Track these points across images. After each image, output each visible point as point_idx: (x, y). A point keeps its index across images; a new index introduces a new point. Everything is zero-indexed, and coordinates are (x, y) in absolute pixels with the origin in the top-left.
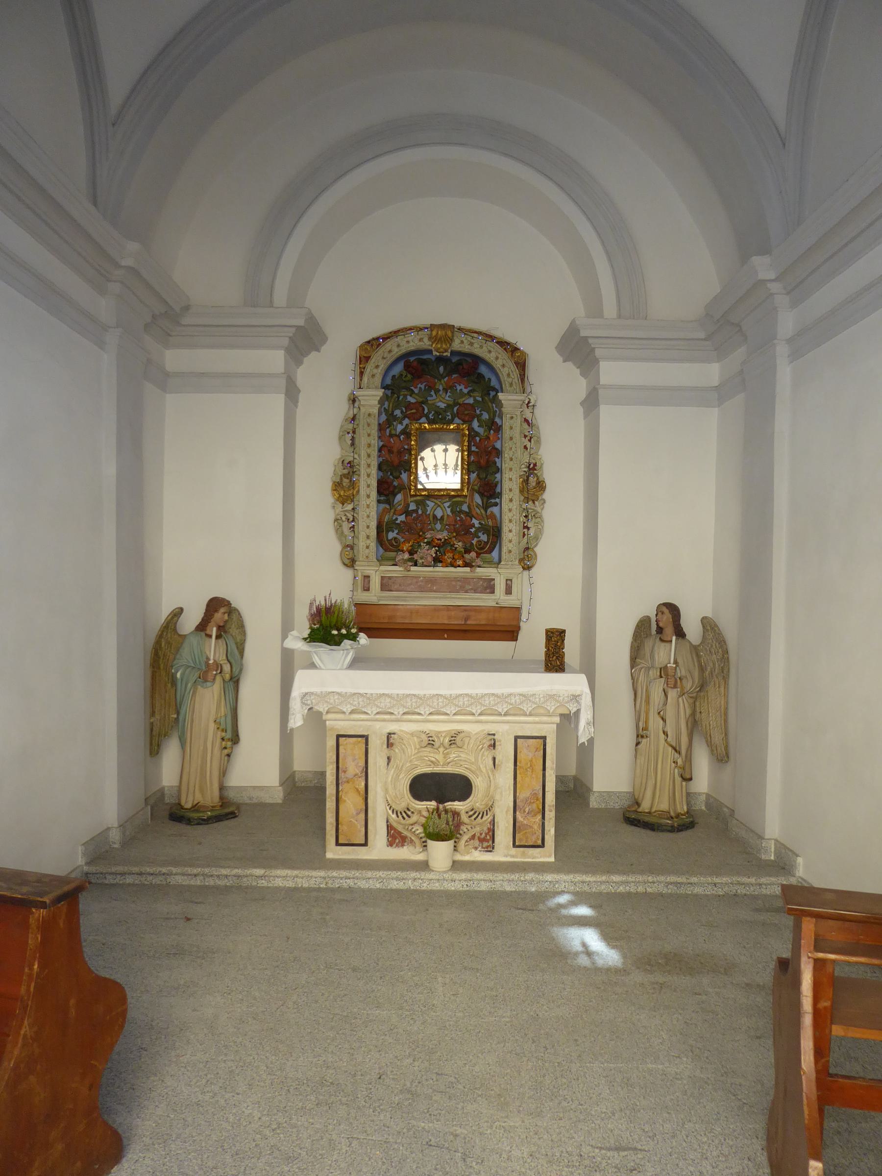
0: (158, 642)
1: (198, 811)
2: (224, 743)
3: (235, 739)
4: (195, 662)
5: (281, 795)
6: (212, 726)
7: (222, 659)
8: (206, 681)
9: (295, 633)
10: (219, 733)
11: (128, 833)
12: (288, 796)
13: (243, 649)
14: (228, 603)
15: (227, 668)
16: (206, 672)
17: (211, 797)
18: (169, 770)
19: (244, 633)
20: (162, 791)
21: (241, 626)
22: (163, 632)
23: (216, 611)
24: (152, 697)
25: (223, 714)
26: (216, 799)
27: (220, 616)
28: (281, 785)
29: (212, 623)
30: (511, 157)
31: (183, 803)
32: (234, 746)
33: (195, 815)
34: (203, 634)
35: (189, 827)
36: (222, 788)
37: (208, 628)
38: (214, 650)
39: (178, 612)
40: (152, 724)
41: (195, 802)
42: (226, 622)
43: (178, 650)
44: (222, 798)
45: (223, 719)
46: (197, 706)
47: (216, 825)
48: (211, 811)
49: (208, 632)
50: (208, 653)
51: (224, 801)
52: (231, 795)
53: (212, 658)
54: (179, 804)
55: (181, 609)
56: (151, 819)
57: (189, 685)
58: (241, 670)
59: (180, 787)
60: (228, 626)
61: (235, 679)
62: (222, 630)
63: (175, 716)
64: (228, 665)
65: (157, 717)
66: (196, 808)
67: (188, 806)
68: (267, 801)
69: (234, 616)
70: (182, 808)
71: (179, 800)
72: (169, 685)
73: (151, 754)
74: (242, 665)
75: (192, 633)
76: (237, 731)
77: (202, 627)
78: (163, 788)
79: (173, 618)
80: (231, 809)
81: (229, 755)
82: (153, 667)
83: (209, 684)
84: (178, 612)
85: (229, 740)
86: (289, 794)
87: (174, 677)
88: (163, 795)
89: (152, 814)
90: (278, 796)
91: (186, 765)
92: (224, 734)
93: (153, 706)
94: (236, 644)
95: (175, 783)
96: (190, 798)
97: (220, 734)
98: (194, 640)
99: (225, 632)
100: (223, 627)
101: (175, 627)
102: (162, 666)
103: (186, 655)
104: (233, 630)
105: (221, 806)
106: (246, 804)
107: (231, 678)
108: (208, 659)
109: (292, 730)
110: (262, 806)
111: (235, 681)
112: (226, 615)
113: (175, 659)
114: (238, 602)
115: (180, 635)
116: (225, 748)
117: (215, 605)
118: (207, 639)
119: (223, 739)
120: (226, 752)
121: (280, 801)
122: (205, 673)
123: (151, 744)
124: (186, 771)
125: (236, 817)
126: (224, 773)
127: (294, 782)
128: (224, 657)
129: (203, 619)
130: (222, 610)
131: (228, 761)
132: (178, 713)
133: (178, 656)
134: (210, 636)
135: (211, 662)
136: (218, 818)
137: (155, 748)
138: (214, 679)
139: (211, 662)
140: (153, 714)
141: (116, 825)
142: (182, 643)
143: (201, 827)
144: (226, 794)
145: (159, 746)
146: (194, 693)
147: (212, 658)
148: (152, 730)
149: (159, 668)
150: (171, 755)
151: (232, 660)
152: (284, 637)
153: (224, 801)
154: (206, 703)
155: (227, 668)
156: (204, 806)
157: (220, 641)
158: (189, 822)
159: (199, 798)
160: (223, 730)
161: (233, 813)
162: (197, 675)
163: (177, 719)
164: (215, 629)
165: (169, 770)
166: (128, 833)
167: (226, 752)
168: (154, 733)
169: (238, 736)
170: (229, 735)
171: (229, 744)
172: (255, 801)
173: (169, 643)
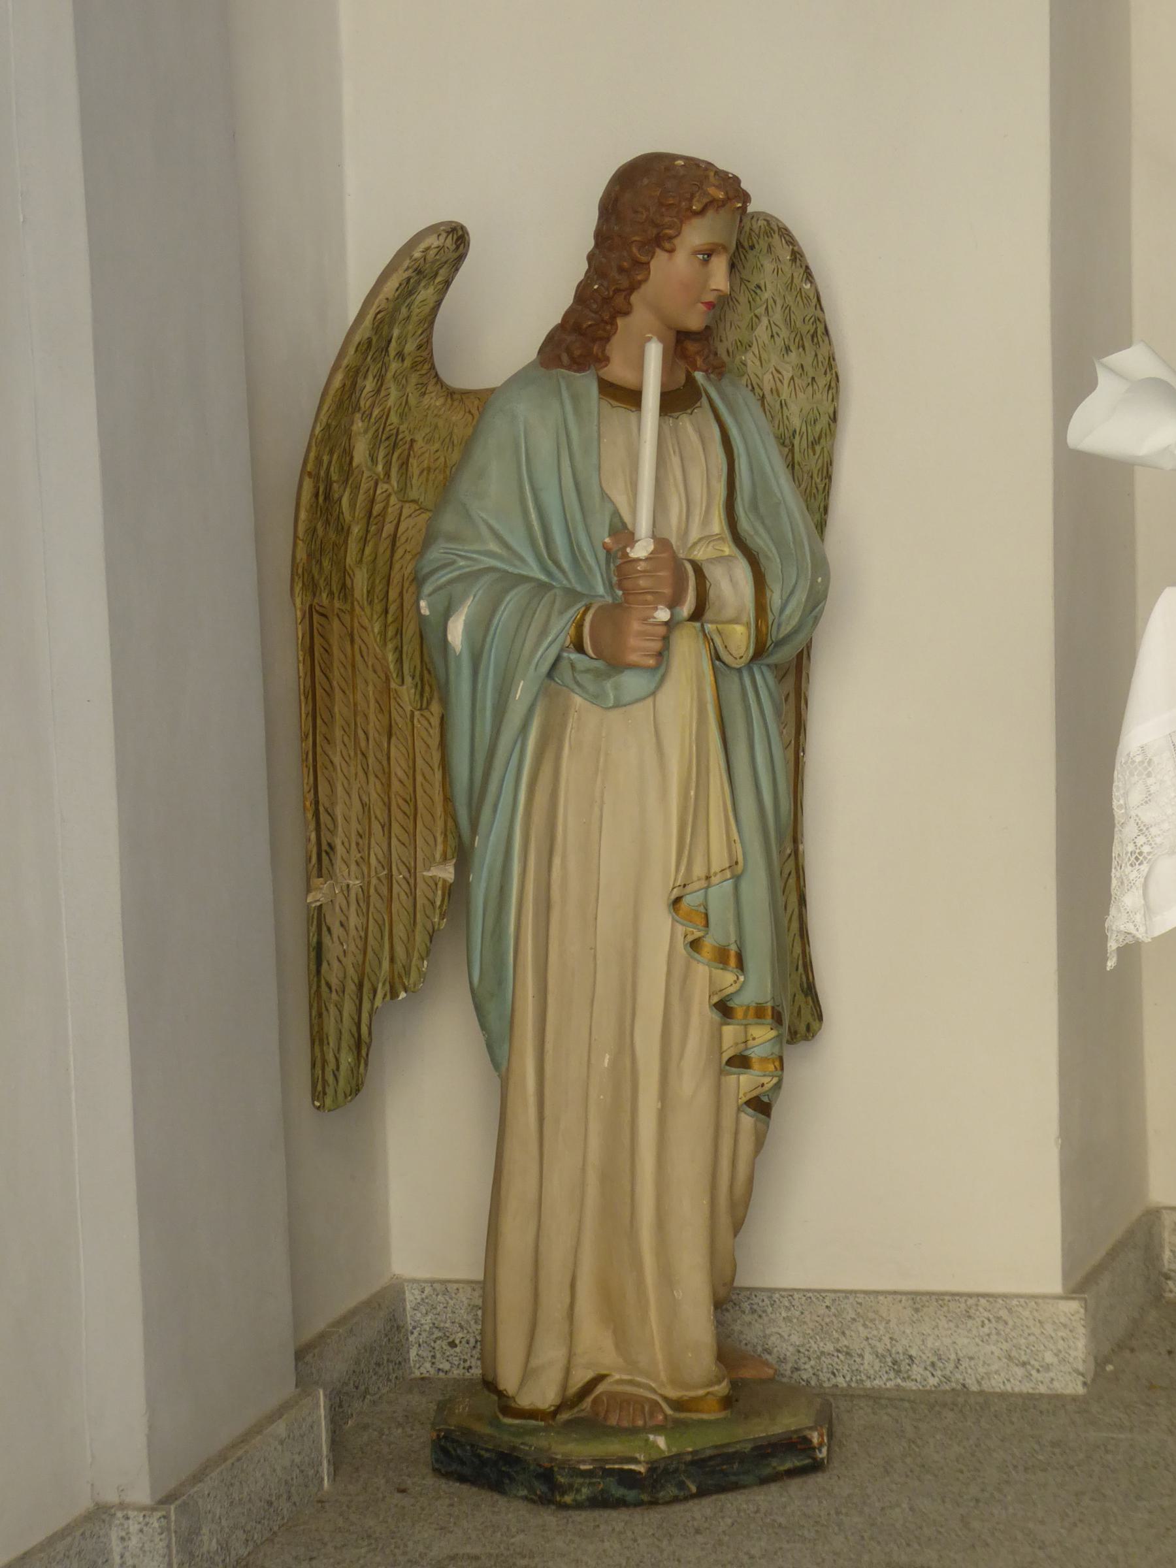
0: (331, 439)
1: (593, 1426)
2: (730, 1032)
3: (798, 1010)
4: (546, 553)
5: (1079, 1348)
6: (660, 932)
7: (703, 534)
8: (616, 665)
9: (1136, 360)
10: (702, 971)
11: (208, 1543)
12: (1114, 1353)
13: (827, 474)
14: (732, 193)
15: (733, 586)
16: (612, 617)
17: (667, 1350)
18: (424, 1187)
19: (827, 375)
20: (386, 1311)
21: (814, 334)
22: (355, 375)
23: (661, 240)
24: (314, 763)
25: (719, 860)
26: (700, 1362)
27: (681, 273)
28: (1082, 1282)
29: (640, 317)
30: (633, 1191)
31: (509, 1380)
32: (793, 1054)
33: (580, 1451)
34: (587, 382)
35: (549, 1518)
36: (727, 1300)
37: (617, 350)
38: (653, 479)
39: (439, 256)
40: (318, 918)
41: (581, 1377)
42: (720, 306)
43: (446, 482)
44: (728, 1355)
45: (720, 894)
46: (695, 704)
47: (701, 1510)
48: (671, 1428)
49: (618, 371)
50: (621, 501)
51: (744, 1376)
52: (783, 1339)
53: (643, 527)
54: (490, 1384)
55: (458, 236)
56: (336, 1466)
57: (521, 693)
58: (816, 602)
59: (487, 1288)
60: (730, 336)
61: (786, 654)
62: (699, 358)
63: (447, 873)
64: (742, 572)
65: (348, 876)
66: (584, 1407)
67: (543, 1394)
68: (996, 1384)
69: (768, 274)
70: (506, 1405)
71: (486, 1346)
72: (407, 693)
73: (318, 1092)
74: (821, 566)
75: (520, 379)
76: (807, 965)
77: (581, 341)
78: (394, 1292)
79: (407, 291)
80: (785, 1423)
81: (761, 1106)
82: (311, 587)
83: (633, 683)
84: (439, 256)
85: (759, 1012)
86: (1122, 1346)
87: (428, 645)
88: (395, 1327)
89: (335, 1443)
90: (1059, 1356)
91: (522, 1155)
92: (728, 979)
93: (318, 813)
94: (785, 441)
95: (464, 1264)
96: (551, 1354)
97: (705, 979)
98: (537, 425)
99: (718, 370)
100: (705, 335)
101: (426, 344)
102: (360, 581)
103: (493, 513)
104: (765, 358)
105: (727, 1402)
106: (875, 1398)
107: (760, 651)
108: (623, 533)
109: (1131, 951)
110: (961, 1408)
111: (782, 667)
112: (719, 266)
113: (428, 541)
114: (789, 184)
115: (453, 395)
116: (741, 1061)
117: (654, 203)
118: (617, 415)
119: (724, 1009)
120: (745, 1083)
121: (1075, 1387)
122: (612, 616)
123: (317, 1038)
124: (520, 1187)
125: (816, 1467)
126: (735, 1210)
127: (1155, 1278)
128: (718, 524)
129: (583, 295)
130: (696, 234)
131: (760, 1142)
132: (463, 857)
133: (449, 522)
134: (632, 397)
135: (641, 550)
136: (716, 1473)
137: (338, 1062)
138: (662, 655)
139: (641, 550)
140: (321, 859)
141: (142, 1494)
142: (468, 446)
143: (617, 1518)
144: (750, 1332)
145: (360, 1046)
146: (551, 738)
147: (643, 527)
148: (318, 953)
149: (345, 591)
150: (429, 1098)
151: (761, 541)
152: (1072, 384)
153: (744, 1376)
154: (619, 797)
155: (733, 586)
156: (623, 1402)
157: (685, 423)
158: (547, 1486)
159: (597, 1350)
160: (721, 957)
161: (797, 1444)
162: (561, 627)
163: (457, 894)
164: (654, 353)
165: (424, 1187)
166: (208, 1543)
167: (745, 1083)
168: (332, 973)
169: (810, 990)
170: (757, 985)
171: (762, 1035)
172: (921, 1378)
173: (392, 443)
